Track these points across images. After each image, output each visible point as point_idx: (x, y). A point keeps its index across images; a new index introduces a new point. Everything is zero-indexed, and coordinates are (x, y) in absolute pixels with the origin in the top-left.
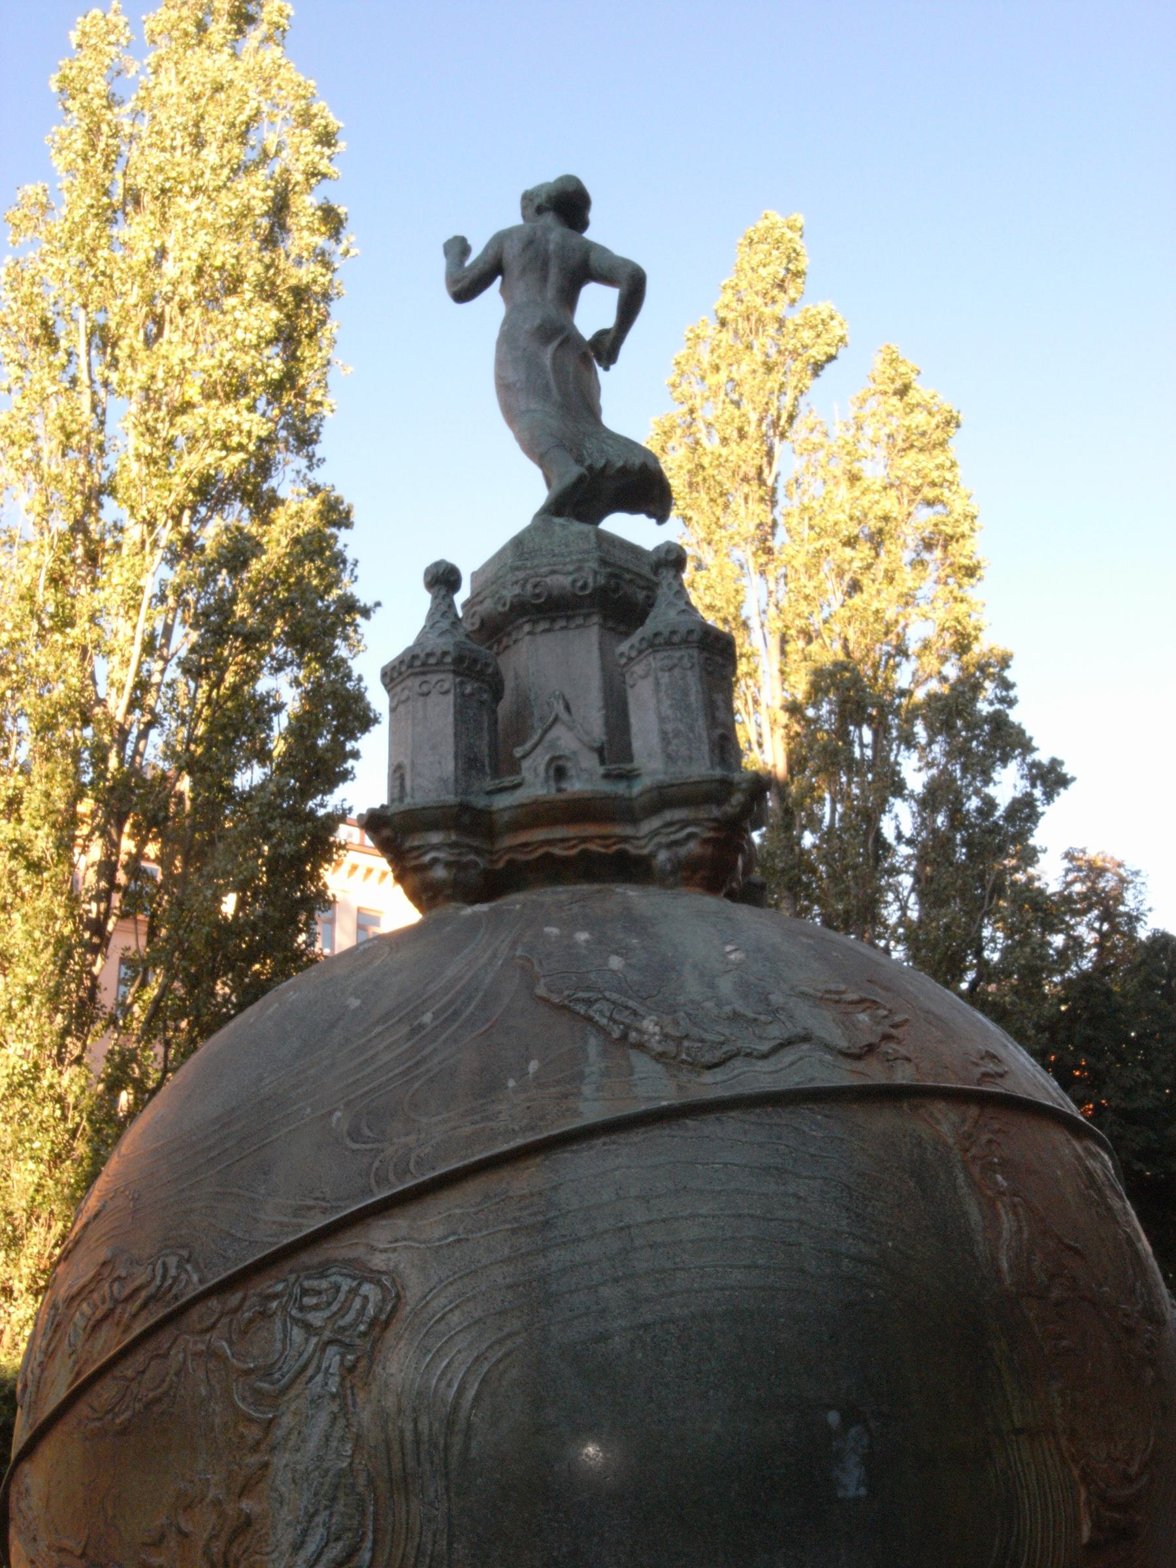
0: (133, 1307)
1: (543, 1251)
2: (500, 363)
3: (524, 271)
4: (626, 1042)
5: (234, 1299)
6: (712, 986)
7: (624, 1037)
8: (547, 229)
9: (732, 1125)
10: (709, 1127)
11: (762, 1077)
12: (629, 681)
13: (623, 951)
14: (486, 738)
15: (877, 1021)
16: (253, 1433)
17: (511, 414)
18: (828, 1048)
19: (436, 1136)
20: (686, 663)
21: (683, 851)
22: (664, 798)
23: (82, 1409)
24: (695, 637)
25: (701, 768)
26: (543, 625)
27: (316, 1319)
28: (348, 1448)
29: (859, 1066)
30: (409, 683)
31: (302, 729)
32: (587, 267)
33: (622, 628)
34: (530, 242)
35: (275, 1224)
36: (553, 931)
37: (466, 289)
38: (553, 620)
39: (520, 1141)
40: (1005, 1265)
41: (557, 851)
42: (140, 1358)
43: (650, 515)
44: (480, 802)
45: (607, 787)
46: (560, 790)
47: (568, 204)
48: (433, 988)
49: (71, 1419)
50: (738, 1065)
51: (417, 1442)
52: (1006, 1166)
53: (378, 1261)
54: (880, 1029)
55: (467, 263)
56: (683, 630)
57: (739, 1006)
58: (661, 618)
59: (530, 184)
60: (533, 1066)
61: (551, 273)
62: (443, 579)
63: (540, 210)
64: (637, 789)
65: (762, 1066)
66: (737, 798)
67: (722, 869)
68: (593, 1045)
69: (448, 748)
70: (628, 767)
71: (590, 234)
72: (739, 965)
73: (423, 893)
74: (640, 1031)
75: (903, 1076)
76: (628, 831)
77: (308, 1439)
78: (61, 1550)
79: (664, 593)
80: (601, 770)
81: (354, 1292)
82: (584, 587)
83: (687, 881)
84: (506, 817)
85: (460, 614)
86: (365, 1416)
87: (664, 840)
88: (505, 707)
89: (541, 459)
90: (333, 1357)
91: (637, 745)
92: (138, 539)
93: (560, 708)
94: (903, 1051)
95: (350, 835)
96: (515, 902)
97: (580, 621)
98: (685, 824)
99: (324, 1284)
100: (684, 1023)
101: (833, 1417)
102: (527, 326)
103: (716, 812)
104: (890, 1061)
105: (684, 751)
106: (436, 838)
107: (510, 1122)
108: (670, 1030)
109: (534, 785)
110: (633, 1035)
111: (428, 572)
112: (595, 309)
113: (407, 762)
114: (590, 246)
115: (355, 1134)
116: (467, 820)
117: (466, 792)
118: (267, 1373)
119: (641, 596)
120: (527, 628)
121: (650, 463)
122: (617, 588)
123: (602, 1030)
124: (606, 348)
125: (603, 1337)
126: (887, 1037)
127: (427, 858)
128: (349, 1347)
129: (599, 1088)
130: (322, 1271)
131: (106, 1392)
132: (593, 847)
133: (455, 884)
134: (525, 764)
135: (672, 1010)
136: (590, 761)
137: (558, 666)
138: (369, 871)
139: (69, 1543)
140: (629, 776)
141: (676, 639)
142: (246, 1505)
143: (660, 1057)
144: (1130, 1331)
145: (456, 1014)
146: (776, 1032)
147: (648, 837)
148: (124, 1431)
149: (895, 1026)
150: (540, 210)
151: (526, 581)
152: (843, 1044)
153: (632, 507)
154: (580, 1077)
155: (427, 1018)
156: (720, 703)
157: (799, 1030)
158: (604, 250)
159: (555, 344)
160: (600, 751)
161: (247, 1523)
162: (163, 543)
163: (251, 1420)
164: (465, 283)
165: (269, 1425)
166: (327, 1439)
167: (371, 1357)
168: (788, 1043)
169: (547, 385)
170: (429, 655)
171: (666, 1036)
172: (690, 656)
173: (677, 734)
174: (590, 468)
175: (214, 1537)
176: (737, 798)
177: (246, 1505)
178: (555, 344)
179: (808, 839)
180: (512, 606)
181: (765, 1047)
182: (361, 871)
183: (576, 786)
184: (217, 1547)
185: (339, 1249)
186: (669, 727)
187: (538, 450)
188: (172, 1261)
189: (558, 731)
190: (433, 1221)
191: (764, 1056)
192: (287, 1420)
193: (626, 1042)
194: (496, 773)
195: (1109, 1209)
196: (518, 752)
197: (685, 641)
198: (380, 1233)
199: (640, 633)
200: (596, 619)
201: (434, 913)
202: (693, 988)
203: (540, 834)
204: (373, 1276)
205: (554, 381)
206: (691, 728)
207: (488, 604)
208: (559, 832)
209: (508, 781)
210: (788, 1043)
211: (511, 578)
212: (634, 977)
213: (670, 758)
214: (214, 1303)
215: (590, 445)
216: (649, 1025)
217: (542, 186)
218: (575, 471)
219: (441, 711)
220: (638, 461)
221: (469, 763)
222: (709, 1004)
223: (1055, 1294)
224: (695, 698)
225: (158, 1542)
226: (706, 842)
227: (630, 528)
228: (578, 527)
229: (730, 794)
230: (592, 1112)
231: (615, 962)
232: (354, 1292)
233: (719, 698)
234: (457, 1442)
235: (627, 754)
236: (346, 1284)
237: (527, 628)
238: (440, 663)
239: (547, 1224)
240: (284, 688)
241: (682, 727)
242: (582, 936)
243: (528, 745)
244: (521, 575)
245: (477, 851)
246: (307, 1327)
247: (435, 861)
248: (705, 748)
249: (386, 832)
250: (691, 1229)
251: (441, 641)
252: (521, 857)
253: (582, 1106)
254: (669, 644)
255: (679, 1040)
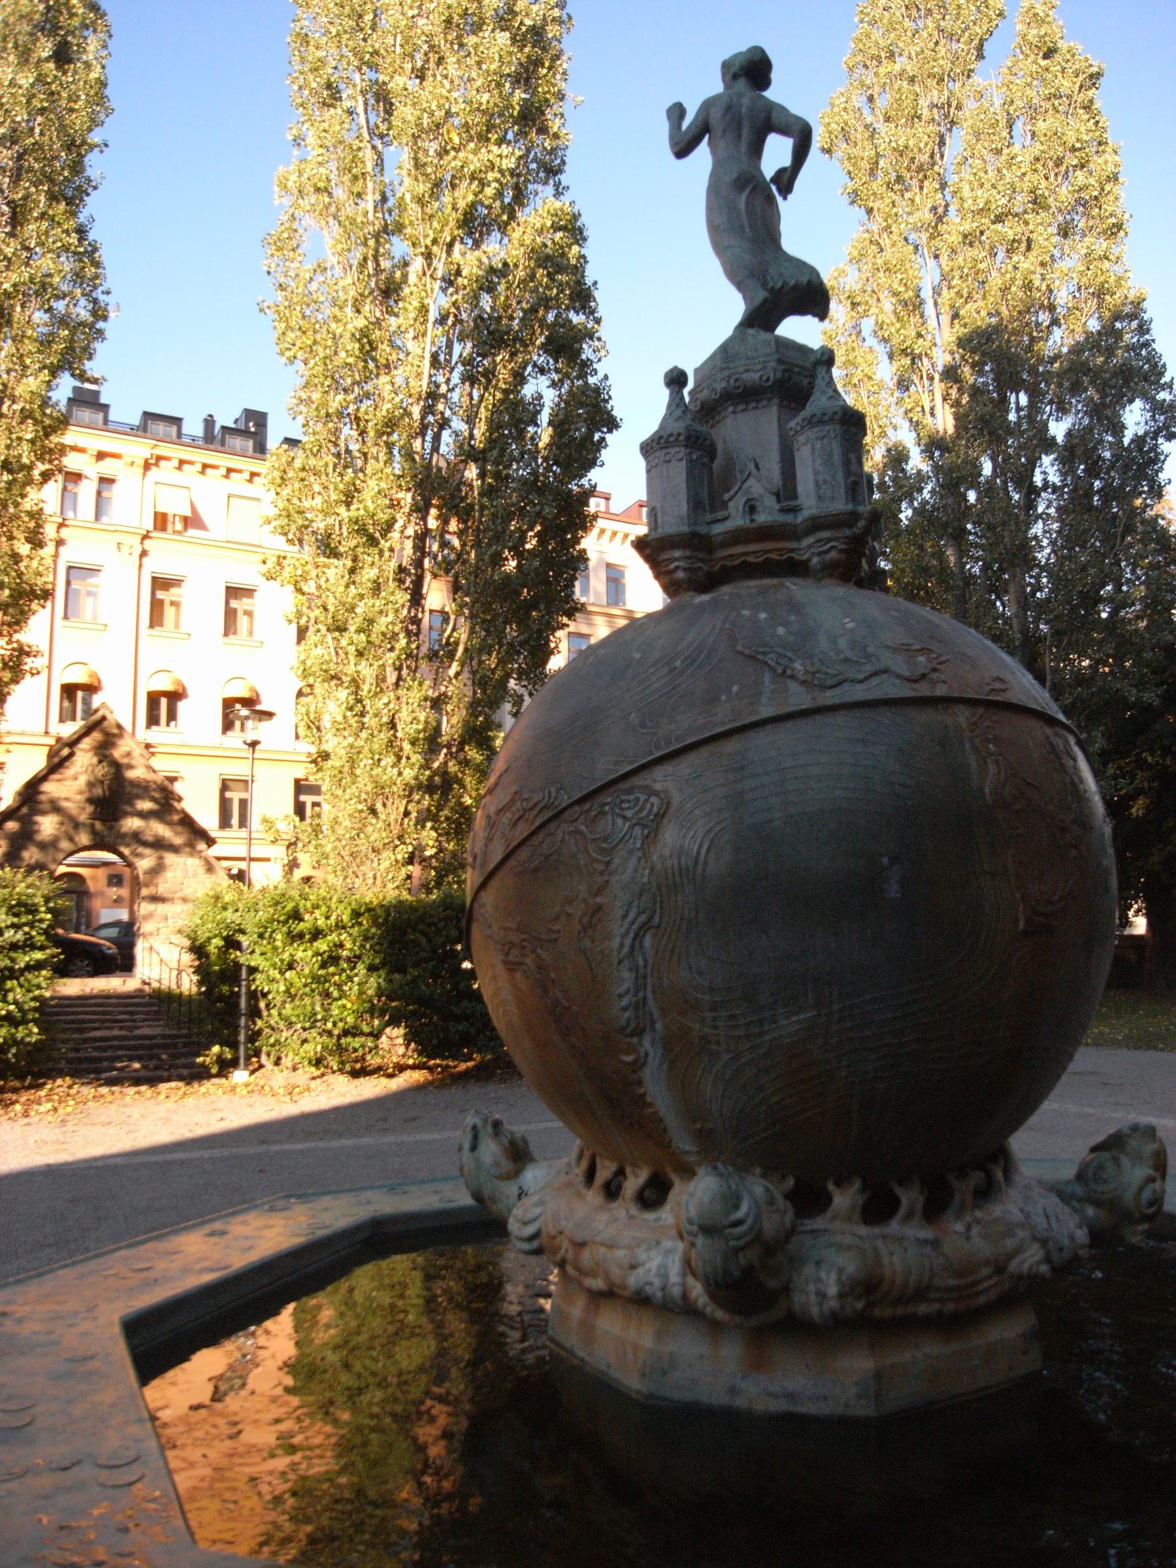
0: (534, 812)
1: (741, 780)
2: (710, 209)
3: (724, 131)
4: (785, 675)
5: (587, 806)
6: (835, 643)
7: (784, 672)
8: (740, 96)
9: (840, 718)
10: (828, 719)
11: (859, 693)
12: (796, 447)
13: (786, 624)
14: (706, 489)
15: (929, 661)
16: (600, 867)
17: (719, 248)
18: (899, 676)
19: (685, 725)
20: (832, 434)
21: (828, 557)
22: (816, 525)
23: (512, 862)
24: (837, 417)
25: (840, 505)
26: (741, 407)
27: (629, 814)
28: (647, 872)
29: (916, 686)
30: (657, 454)
31: (560, 424)
32: (771, 120)
33: (793, 405)
34: (729, 108)
35: (605, 768)
36: (746, 612)
37: (683, 149)
38: (747, 403)
39: (728, 727)
40: (987, 790)
41: (750, 559)
42: (541, 835)
43: (814, 315)
44: (702, 530)
45: (782, 518)
46: (752, 521)
47: (753, 70)
48: (680, 648)
49: (505, 871)
50: (846, 687)
51: (680, 868)
52: (996, 740)
53: (658, 786)
54: (930, 666)
55: (685, 124)
56: (830, 412)
57: (849, 654)
58: (818, 403)
59: (726, 55)
60: (735, 688)
61: (742, 128)
62: (676, 379)
63: (735, 77)
64: (799, 520)
65: (858, 687)
66: (861, 524)
67: (854, 569)
68: (767, 677)
69: (683, 495)
70: (794, 503)
71: (770, 94)
72: (851, 631)
73: (671, 588)
74: (793, 669)
75: (941, 691)
76: (794, 545)
77: (627, 871)
78: (506, 929)
79: (820, 383)
80: (777, 507)
81: (646, 801)
82: (768, 380)
83: (830, 576)
84: (719, 539)
85: (687, 399)
86: (655, 858)
87: (816, 551)
88: (717, 465)
89: (739, 286)
90: (638, 831)
91: (800, 489)
92: (420, 269)
93: (751, 466)
94: (943, 677)
95: (598, 505)
96: (726, 590)
97: (765, 403)
98: (829, 540)
99: (632, 797)
100: (818, 665)
101: (885, 861)
102: (728, 179)
103: (847, 532)
104: (934, 683)
105: (829, 494)
106: (677, 554)
107: (723, 717)
108: (809, 668)
109: (737, 520)
110: (789, 672)
111: (666, 375)
112: (777, 152)
113: (658, 506)
114: (771, 106)
115: (643, 725)
116: (696, 542)
117: (695, 524)
118: (606, 839)
119: (806, 382)
120: (731, 409)
121: (814, 278)
122: (790, 378)
123: (773, 670)
124: (786, 180)
125: (770, 821)
126: (934, 670)
127: (672, 566)
128: (645, 826)
129: (770, 699)
130: (630, 791)
131: (524, 853)
132: (772, 556)
133: (689, 581)
134: (731, 504)
135: (811, 657)
136: (770, 501)
137: (751, 434)
138: (614, 534)
139: (508, 925)
140: (795, 510)
141: (826, 418)
142: (599, 900)
143: (803, 683)
144: (1063, 829)
145: (694, 661)
146: (869, 668)
147: (808, 548)
148: (536, 870)
149: (941, 663)
150: (735, 77)
151: (729, 377)
152: (907, 674)
153: (801, 311)
154: (760, 694)
155: (678, 663)
156: (854, 460)
157: (882, 667)
158: (783, 109)
159: (747, 191)
160: (777, 495)
161: (599, 908)
162: (439, 274)
163: (598, 861)
164: (683, 145)
165: (608, 863)
166: (636, 870)
167: (657, 830)
168: (876, 674)
169: (742, 226)
170: (670, 435)
171: (807, 672)
172: (833, 429)
173: (825, 482)
174: (771, 290)
175: (584, 914)
176: (861, 524)
177: (599, 900)
178: (747, 191)
179: (972, 496)
180: (721, 396)
181: (861, 676)
182: (608, 534)
183: (762, 518)
184: (586, 919)
185: (637, 781)
186: (820, 478)
187: (738, 276)
188: (553, 790)
189: (751, 482)
190: (685, 766)
191: (861, 682)
192: (617, 861)
193: (785, 675)
194: (713, 509)
195: (1062, 765)
196: (726, 497)
197: (831, 420)
198: (659, 773)
199: (803, 414)
200: (775, 401)
201: (677, 599)
202: (823, 643)
203: (739, 549)
204: (656, 793)
205: (746, 218)
206: (834, 478)
207: (705, 393)
208: (752, 548)
209: (720, 515)
210: (876, 674)
211: (720, 376)
212: (791, 639)
213: (820, 498)
214: (577, 808)
215: (773, 271)
216: (798, 666)
217: (737, 55)
218: (762, 294)
219: (678, 472)
220: (804, 280)
221: (696, 505)
222: (831, 654)
223: (1017, 807)
224: (837, 458)
225: (556, 919)
226: (841, 551)
227: (798, 329)
228: (764, 335)
229: (857, 521)
230: (765, 712)
231: (781, 631)
232: (646, 801)
233: (853, 457)
234: (700, 867)
235: (794, 495)
236: (643, 798)
237: (731, 409)
238: (677, 440)
239: (742, 768)
240: (542, 389)
241: (828, 478)
242: (763, 616)
243: (732, 492)
244: (726, 373)
245: (702, 561)
246: (625, 818)
247: (677, 568)
248: (842, 491)
249: (648, 551)
250: (816, 769)
251: (677, 425)
252: (729, 564)
253: (762, 709)
254: (821, 422)
255: (814, 673)
